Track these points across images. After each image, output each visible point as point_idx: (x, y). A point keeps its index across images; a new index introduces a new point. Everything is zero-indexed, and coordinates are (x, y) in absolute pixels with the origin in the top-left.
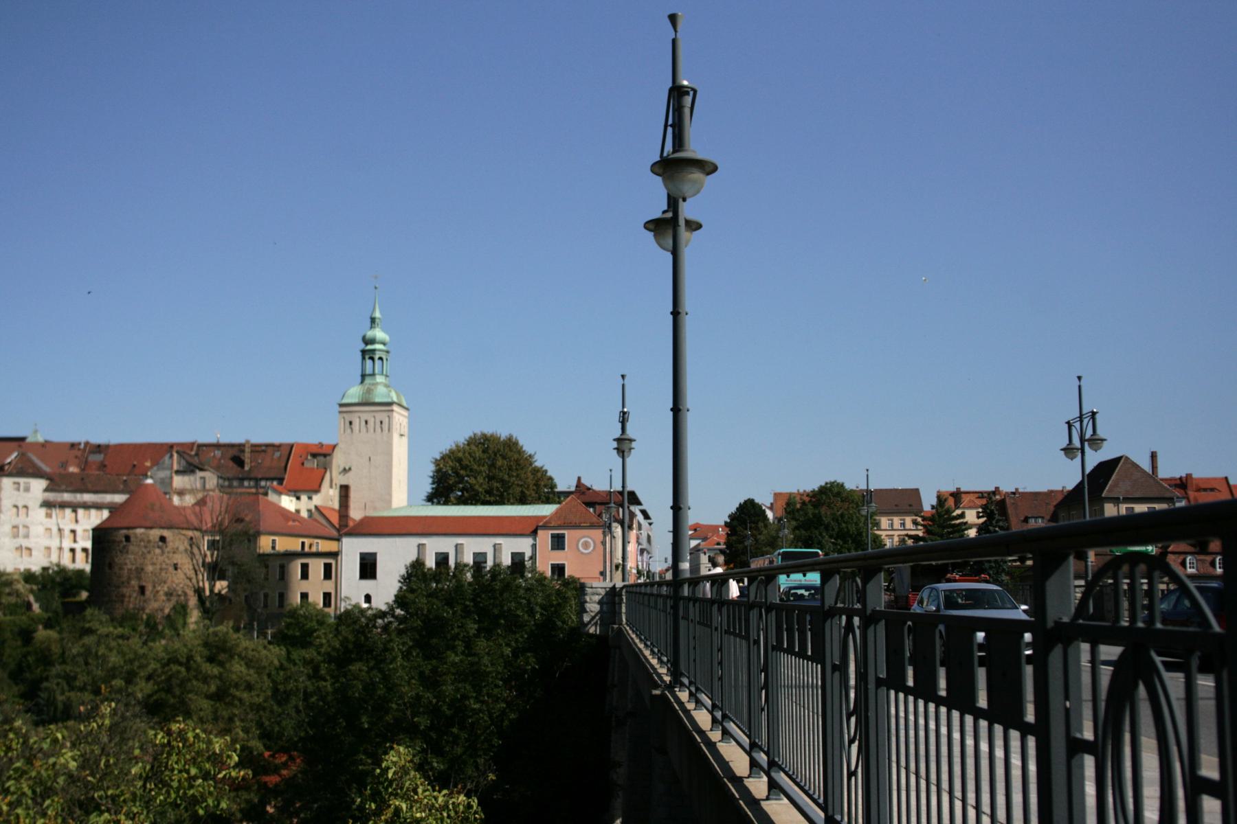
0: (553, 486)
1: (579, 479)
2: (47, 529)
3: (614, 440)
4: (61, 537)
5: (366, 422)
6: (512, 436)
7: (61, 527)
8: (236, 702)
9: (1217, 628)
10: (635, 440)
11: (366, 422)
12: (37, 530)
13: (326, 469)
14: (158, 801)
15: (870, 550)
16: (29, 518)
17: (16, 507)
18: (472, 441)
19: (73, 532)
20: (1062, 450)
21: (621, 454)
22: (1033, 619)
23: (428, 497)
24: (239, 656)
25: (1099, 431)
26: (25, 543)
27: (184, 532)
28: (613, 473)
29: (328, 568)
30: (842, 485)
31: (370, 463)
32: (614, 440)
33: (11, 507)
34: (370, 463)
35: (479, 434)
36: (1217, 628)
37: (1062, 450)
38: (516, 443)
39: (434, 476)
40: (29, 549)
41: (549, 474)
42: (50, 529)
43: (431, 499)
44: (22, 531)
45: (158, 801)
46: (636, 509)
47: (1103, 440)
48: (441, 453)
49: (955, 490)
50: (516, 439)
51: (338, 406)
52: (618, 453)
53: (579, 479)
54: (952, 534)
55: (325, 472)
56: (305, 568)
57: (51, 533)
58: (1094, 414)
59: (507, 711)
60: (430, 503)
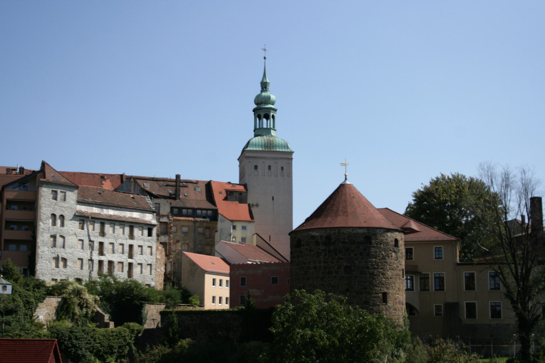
2: (80, 240)
4: (261, 109)
5: (282, 168)
7: (92, 239)
11: (282, 168)
12: (71, 240)
14: (290, 335)
16: (65, 228)
17: (54, 216)
19: (101, 244)
24: (106, 353)
26: (62, 254)
27: (24, 339)
31: (273, 202)
33: (50, 216)
34: (273, 202)
40: (65, 260)
42: (82, 240)
44: (59, 240)
45: (290, 335)
51: (138, 246)
53: (451, 173)
57: (83, 244)
59: (494, 257)
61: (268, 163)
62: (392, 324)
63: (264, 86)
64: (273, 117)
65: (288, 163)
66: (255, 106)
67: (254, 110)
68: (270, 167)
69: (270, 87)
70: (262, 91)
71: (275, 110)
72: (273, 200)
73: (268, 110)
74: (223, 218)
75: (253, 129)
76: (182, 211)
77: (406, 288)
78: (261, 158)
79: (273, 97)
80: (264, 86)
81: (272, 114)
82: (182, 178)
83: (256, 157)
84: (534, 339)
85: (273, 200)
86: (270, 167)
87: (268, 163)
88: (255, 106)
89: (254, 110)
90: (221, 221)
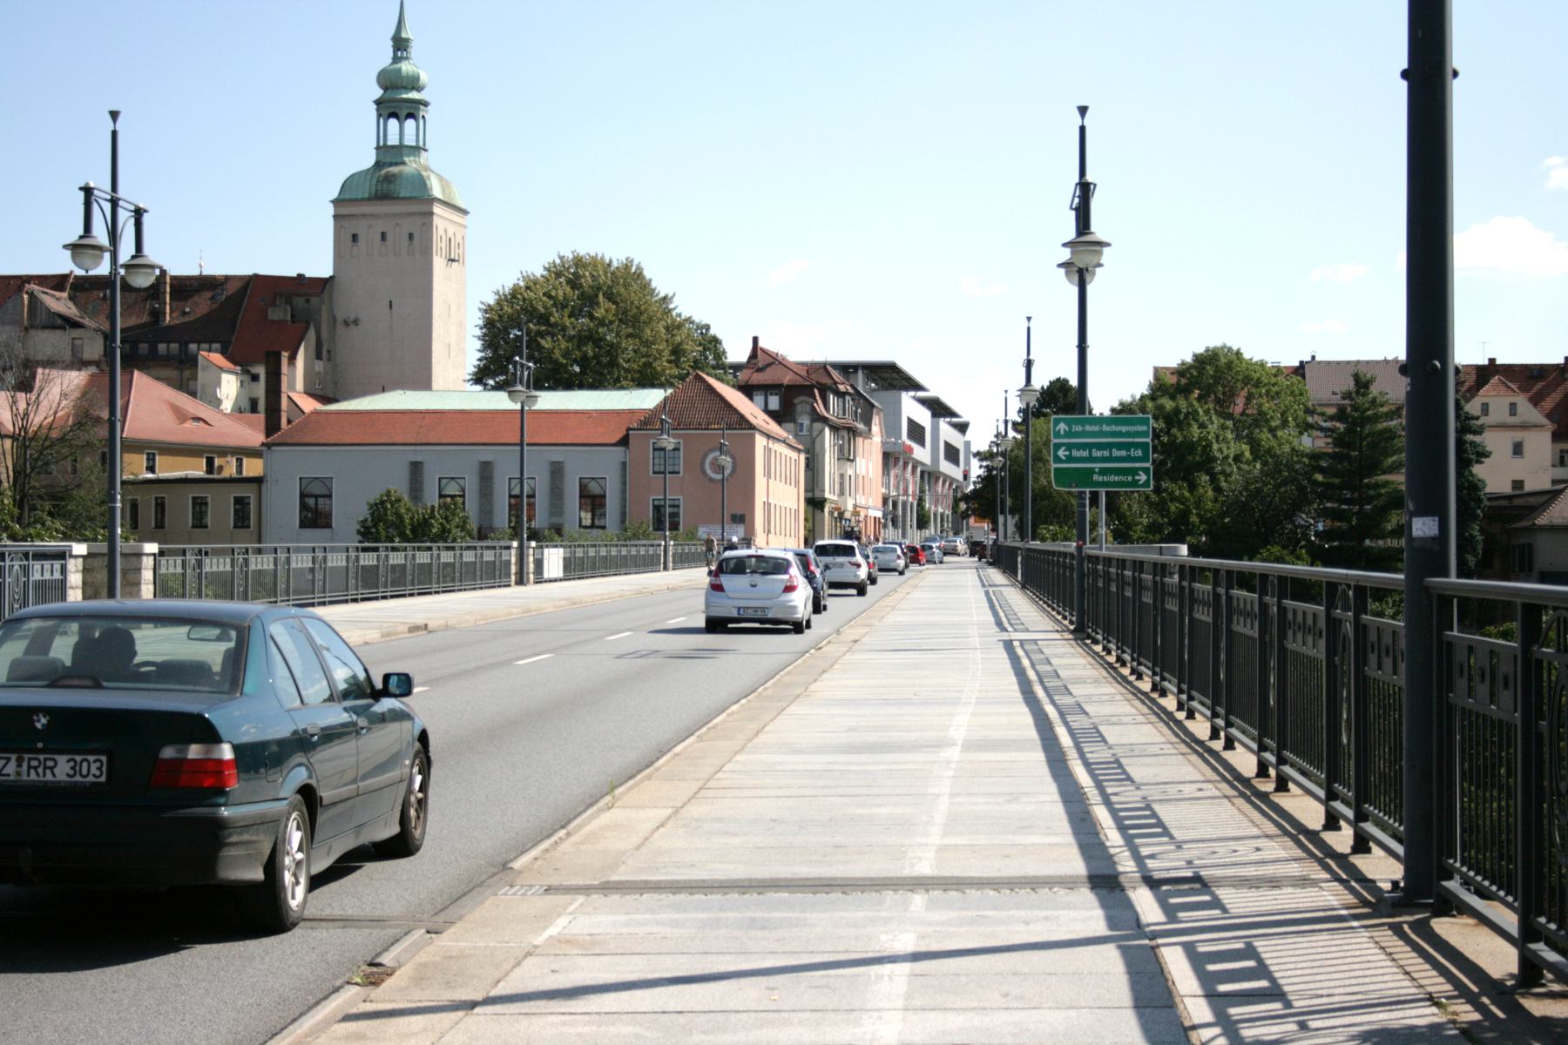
0: (719, 355)
1: (755, 340)
3: (1065, 245)
5: (411, 236)
6: (632, 261)
8: (914, 861)
9: (1501, 1015)
10: (1108, 245)
11: (411, 236)
13: (308, 324)
15: (1104, 551)
18: (555, 272)
20: (1060, 266)
21: (1076, 278)
22: (168, 753)
23: (475, 374)
25: (146, 250)
28: (1032, 324)
29: (241, 502)
30: (1238, 353)
32: (1065, 245)
35: (571, 257)
36: (1501, 1015)
37: (1060, 266)
38: (639, 275)
39: (485, 335)
41: (712, 332)
43: (479, 378)
46: (911, 408)
47: (1101, 244)
48: (497, 293)
49: (1486, 363)
50: (639, 267)
52: (1068, 274)
54: (1347, 504)
55: (307, 329)
56: (200, 504)
58: (138, 213)
60: (479, 387)
61: (379, 226)
62: (314, 576)
63: (400, 45)
64: (423, 117)
65: (424, 224)
66: (379, 93)
67: (378, 103)
68: (383, 236)
69: (415, 50)
70: (396, 60)
71: (426, 104)
72: (391, 307)
73: (413, 105)
74: (206, 363)
75: (375, 145)
76: (157, 347)
77: (264, 487)
78: (364, 216)
79: (424, 78)
80: (400, 45)
81: (421, 114)
82: (1498, 362)
83: (353, 216)
84: (1158, 537)
85: (391, 307)
86: (383, 236)
87: (379, 226)
88: (379, 93)
89: (378, 103)
90: (203, 369)
